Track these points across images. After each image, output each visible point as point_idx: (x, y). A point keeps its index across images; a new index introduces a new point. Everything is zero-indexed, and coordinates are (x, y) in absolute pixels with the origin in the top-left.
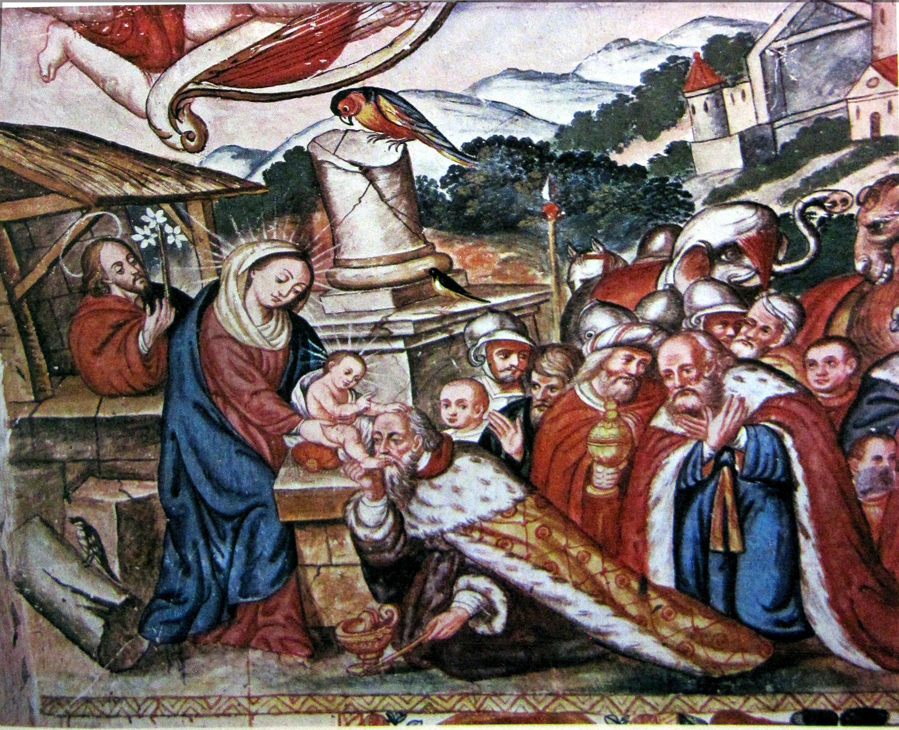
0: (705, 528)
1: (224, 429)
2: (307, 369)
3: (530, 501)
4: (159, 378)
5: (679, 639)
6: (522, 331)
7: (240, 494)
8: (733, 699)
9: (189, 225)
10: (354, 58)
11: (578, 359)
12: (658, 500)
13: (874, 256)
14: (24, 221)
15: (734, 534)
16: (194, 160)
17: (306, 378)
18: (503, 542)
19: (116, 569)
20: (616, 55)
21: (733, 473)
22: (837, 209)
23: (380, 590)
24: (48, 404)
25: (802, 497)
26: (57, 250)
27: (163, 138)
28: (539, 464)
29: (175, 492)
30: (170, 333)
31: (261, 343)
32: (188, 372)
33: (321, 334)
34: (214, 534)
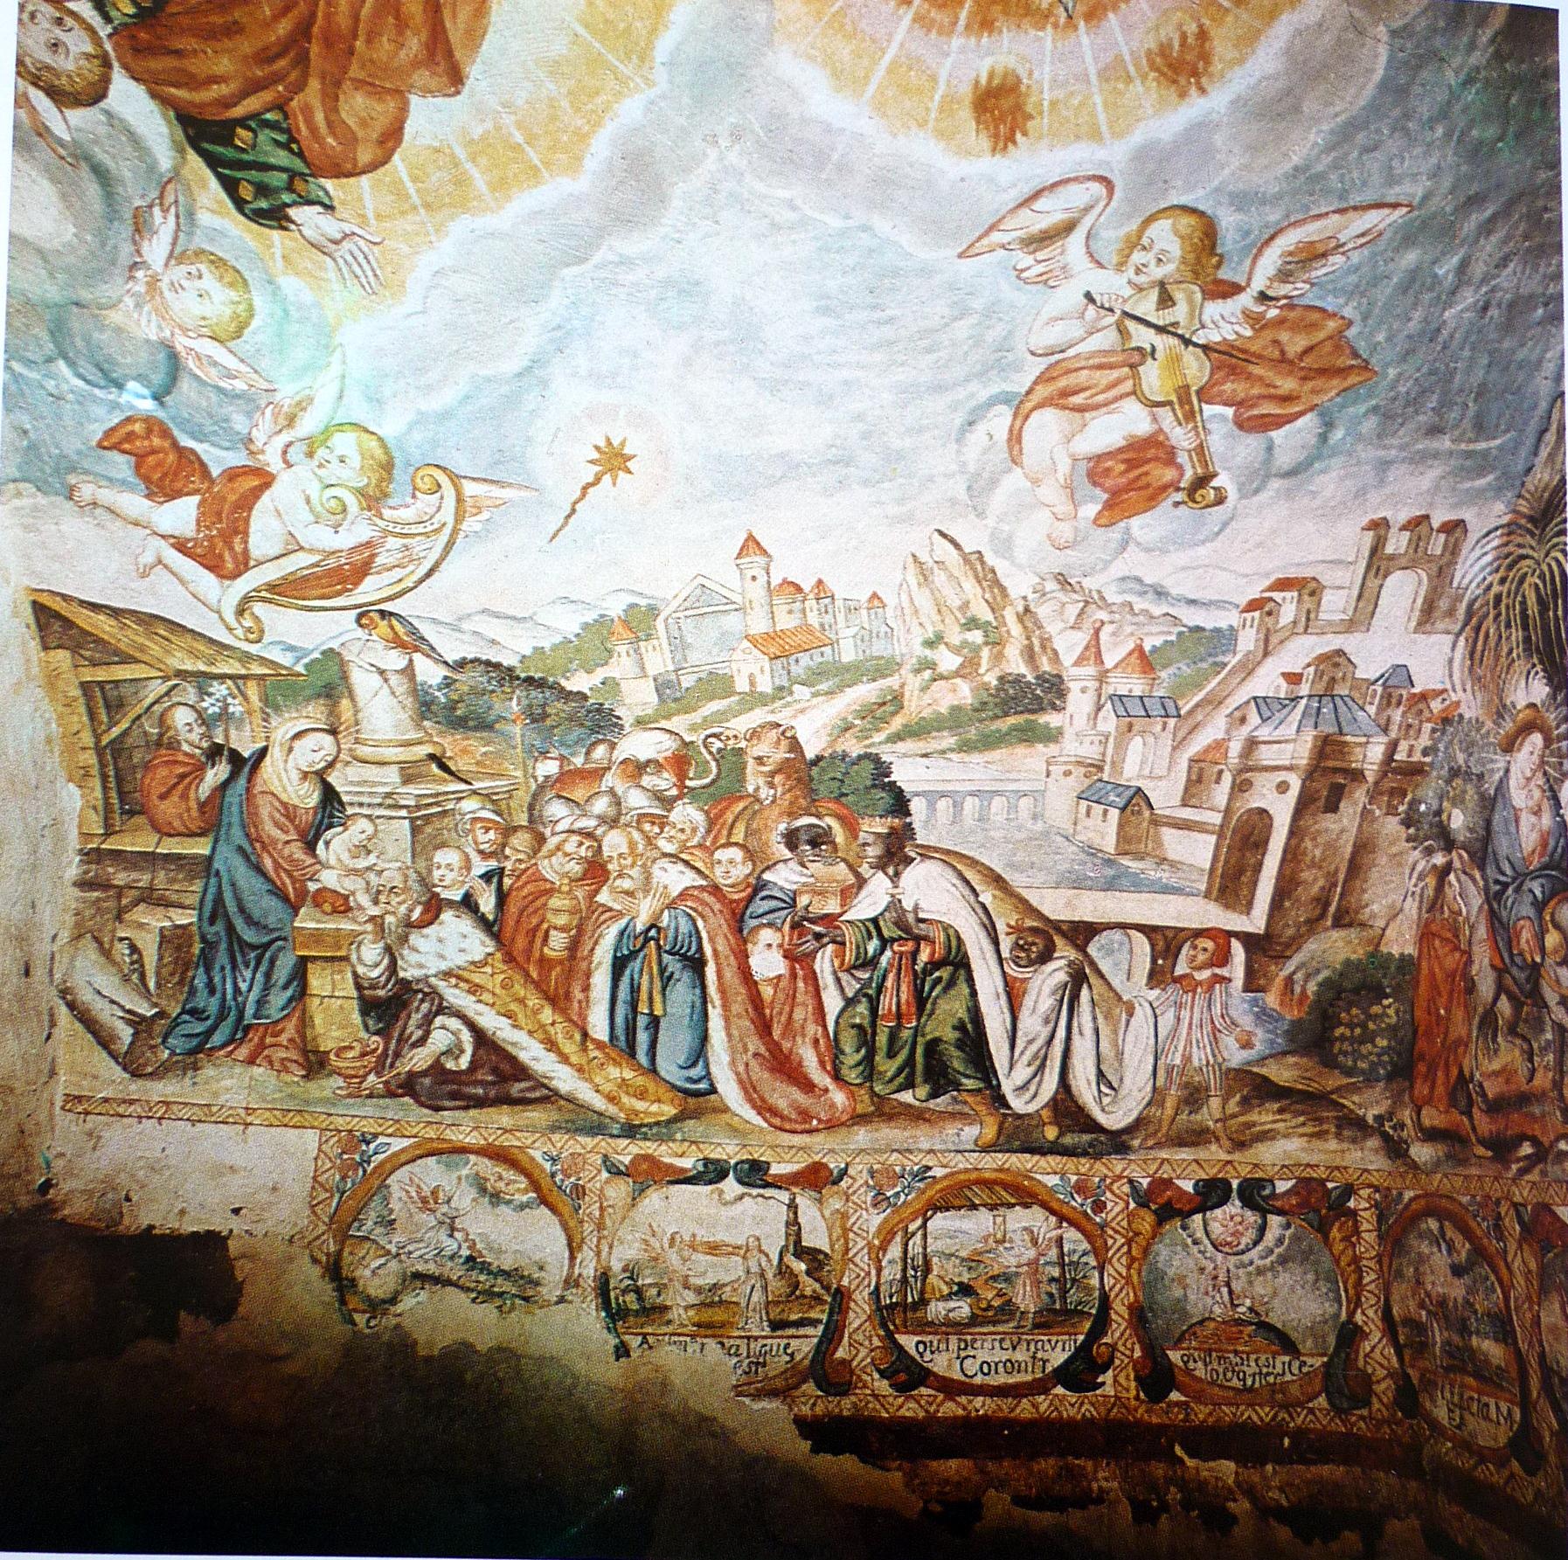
0: (635, 990)
1: (259, 870)
2: (330, 826)
3: (499, 955)
4: (211, 819)
5: (607, 1087)
6: (499, 814)
7: (265, 927)
8: (648, 1144)
9: (246, 698)
10: (369, 590)
11: (541, 839)
12: (600, 963)
13: (761, 781)
14: (116, 682)
15: (657, 998)
16: (253, 649)
17: (328, 834)
18: (475, 989)
19: (152, 985)
20: (559, 608)
21: (659, 947)
22: (731, 742)
23: (371, 1022)
24: (112, 839)
25: (710, 971)
26: (138, 710)
27: (230, 629)
28: (509, 923)
29: (212, 922)
30: (225, 785)
31: (296, 801)
32: (235, 820)
33: (345, 799)
34: (239, 959)
